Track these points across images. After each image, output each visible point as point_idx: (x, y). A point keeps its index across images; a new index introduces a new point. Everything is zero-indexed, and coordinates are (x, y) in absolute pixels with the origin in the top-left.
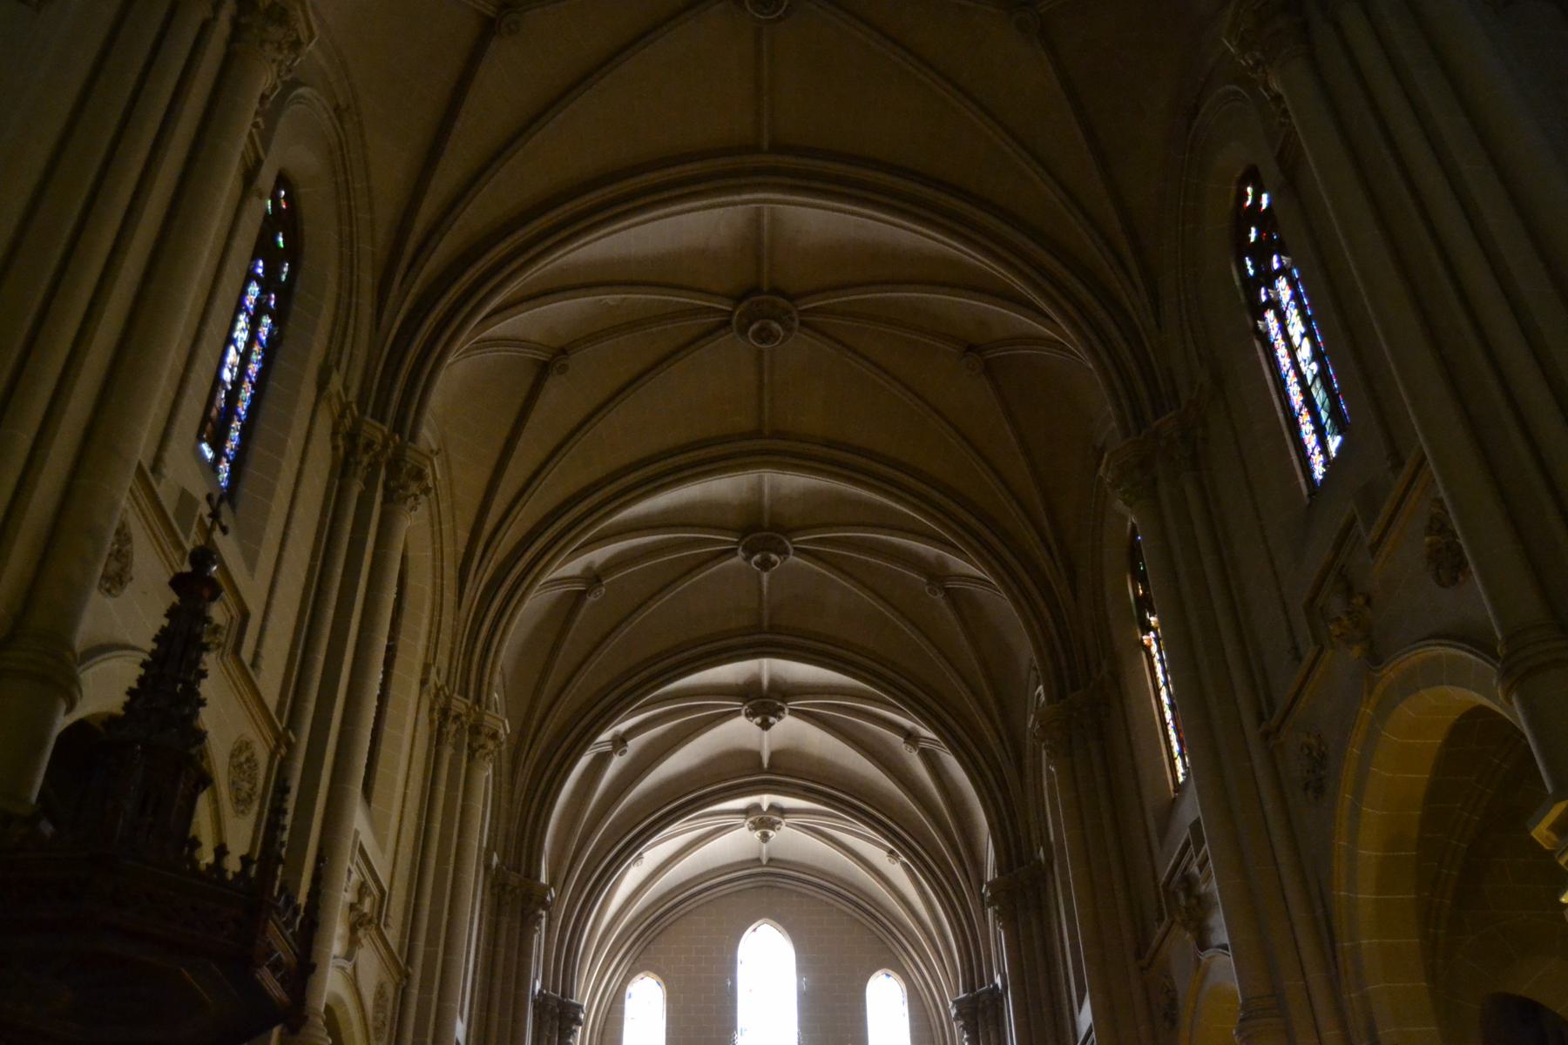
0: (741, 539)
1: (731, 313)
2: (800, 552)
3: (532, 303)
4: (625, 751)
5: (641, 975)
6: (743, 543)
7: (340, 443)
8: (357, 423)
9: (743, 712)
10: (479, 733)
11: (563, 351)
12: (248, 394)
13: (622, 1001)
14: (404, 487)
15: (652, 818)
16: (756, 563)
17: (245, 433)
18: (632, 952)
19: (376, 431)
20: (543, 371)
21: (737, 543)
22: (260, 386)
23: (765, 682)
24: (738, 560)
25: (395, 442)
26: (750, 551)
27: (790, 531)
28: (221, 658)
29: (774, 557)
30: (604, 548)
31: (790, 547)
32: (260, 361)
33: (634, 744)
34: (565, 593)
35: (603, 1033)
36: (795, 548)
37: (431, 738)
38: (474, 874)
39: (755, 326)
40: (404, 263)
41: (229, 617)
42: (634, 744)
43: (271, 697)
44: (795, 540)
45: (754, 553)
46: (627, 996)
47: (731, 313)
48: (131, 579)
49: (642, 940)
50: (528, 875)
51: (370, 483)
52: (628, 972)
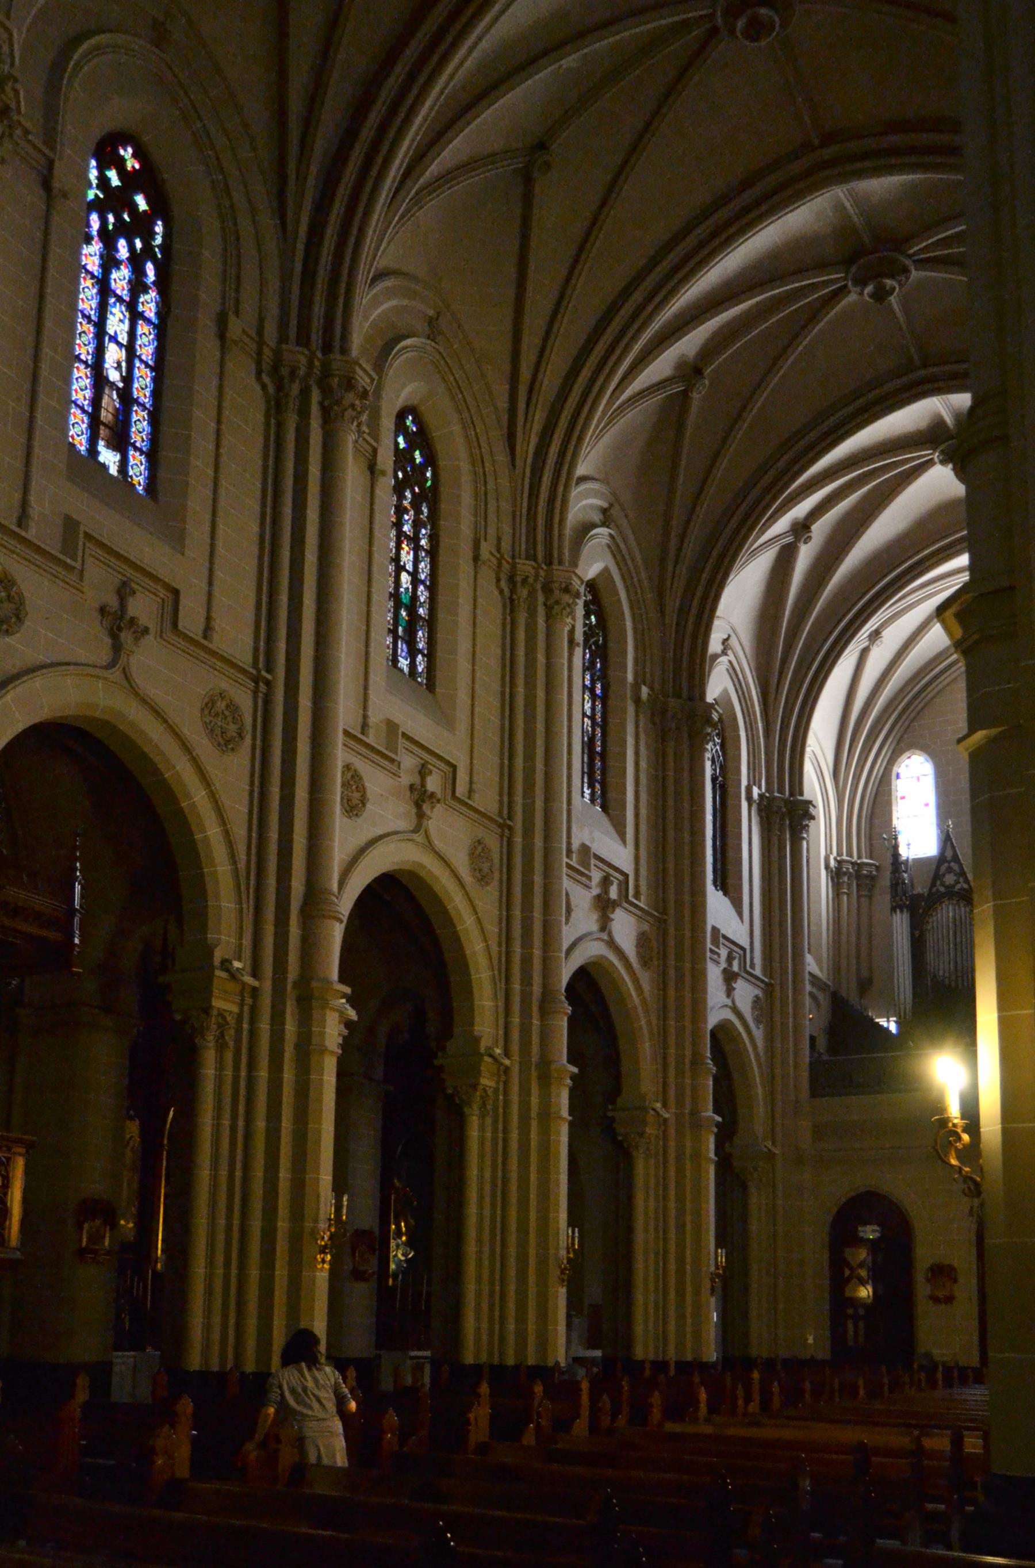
0: (847, 272)
1: (711, 17)
2: (923, 264)
3: (469, 116)
4: (810, 538)
5: (907, 754)
6: (850, 275)
7: (266, 379)
8: (277, 353)
9: (936, 460)
10: (551, 591)
11: (542, 146)
12: (148, 379)
13: (889, 784)
14: (338, 403)
15: (868, 597)
16: (871, 296)
17: (154, 419)
18: (894, 734)
19: (298, 357)
20: (527, 179)
21: (845, 279)
22: (158, 368)
23: (949, 420)
24: (852, 297)
25: (319, 360)
26: (861, 283)
27: (900, 243)
28: (161, 637)
29: (889, 282)
30: (694, 332)
31: (908, 262)
32: (153, 340)
33: (820, 529)
34: (667, 397)
35: (871, 817)
36: (914, 261)
37: (504, 606)
38: (776, 673)
39: (741, 24)
40: (293, 149)
41: (160, 601)
42: (820, 529)
43: (758, 972)
44: (912, 251)
45: (865, 284)
46: (894, 776)
47: (711, 17)
48: (27, 614)
49: (904, 717)
50: (691, 699)
51: (304, 414)
52: (893, 752)
